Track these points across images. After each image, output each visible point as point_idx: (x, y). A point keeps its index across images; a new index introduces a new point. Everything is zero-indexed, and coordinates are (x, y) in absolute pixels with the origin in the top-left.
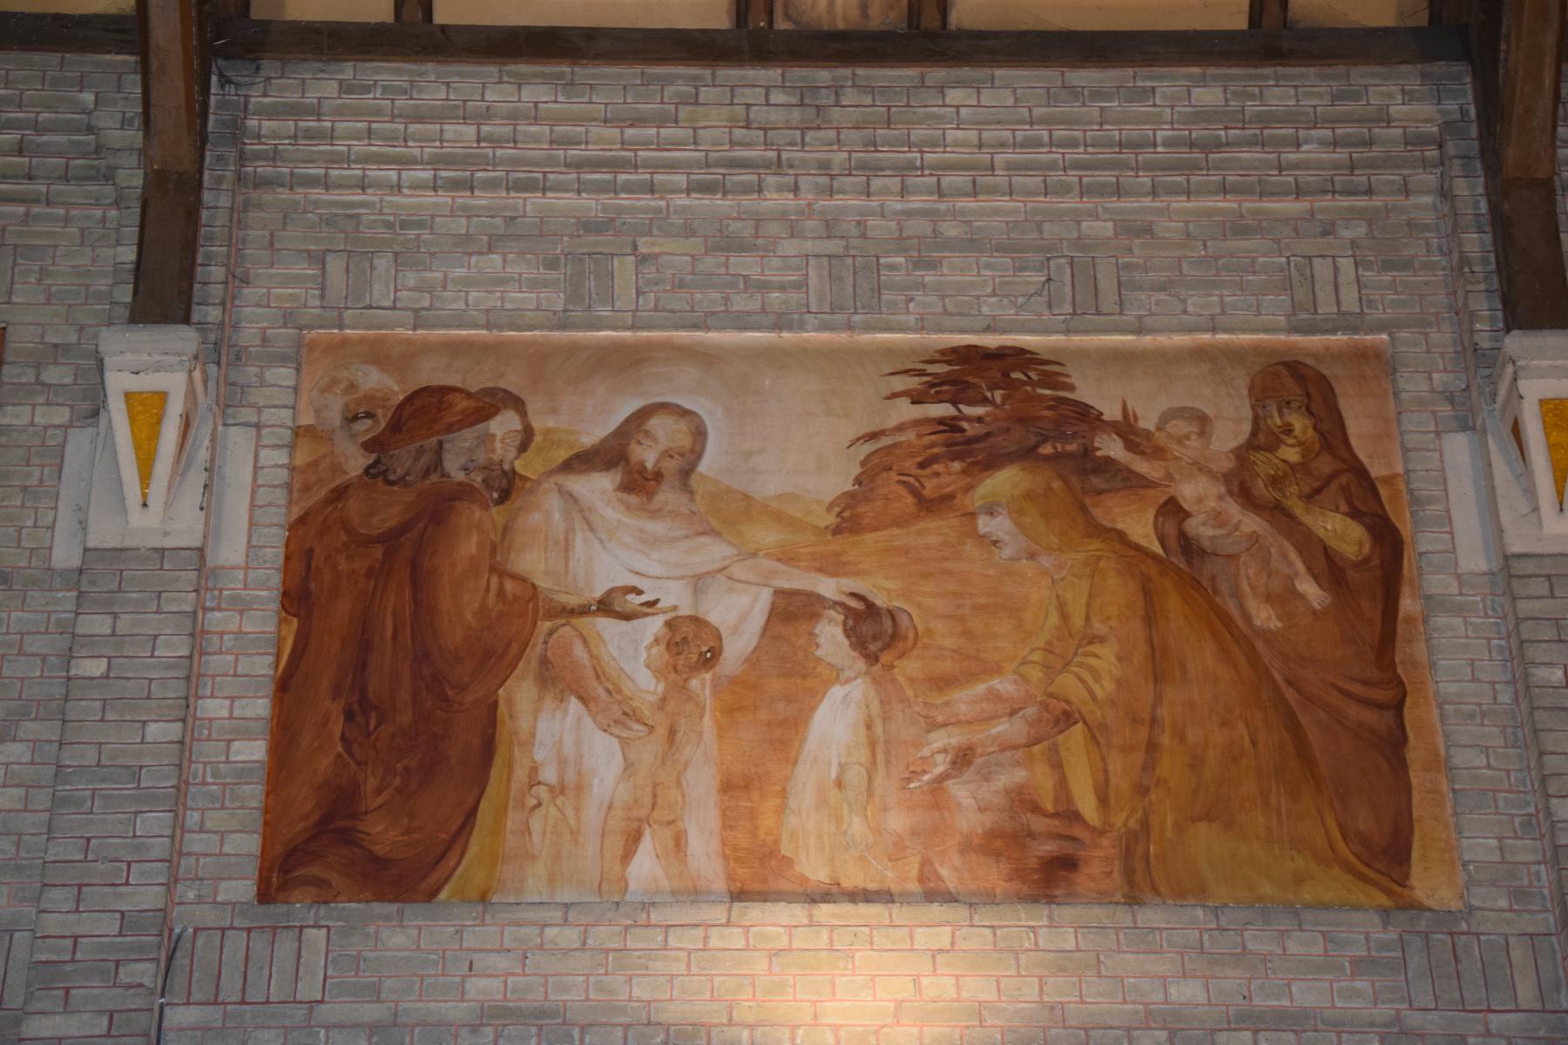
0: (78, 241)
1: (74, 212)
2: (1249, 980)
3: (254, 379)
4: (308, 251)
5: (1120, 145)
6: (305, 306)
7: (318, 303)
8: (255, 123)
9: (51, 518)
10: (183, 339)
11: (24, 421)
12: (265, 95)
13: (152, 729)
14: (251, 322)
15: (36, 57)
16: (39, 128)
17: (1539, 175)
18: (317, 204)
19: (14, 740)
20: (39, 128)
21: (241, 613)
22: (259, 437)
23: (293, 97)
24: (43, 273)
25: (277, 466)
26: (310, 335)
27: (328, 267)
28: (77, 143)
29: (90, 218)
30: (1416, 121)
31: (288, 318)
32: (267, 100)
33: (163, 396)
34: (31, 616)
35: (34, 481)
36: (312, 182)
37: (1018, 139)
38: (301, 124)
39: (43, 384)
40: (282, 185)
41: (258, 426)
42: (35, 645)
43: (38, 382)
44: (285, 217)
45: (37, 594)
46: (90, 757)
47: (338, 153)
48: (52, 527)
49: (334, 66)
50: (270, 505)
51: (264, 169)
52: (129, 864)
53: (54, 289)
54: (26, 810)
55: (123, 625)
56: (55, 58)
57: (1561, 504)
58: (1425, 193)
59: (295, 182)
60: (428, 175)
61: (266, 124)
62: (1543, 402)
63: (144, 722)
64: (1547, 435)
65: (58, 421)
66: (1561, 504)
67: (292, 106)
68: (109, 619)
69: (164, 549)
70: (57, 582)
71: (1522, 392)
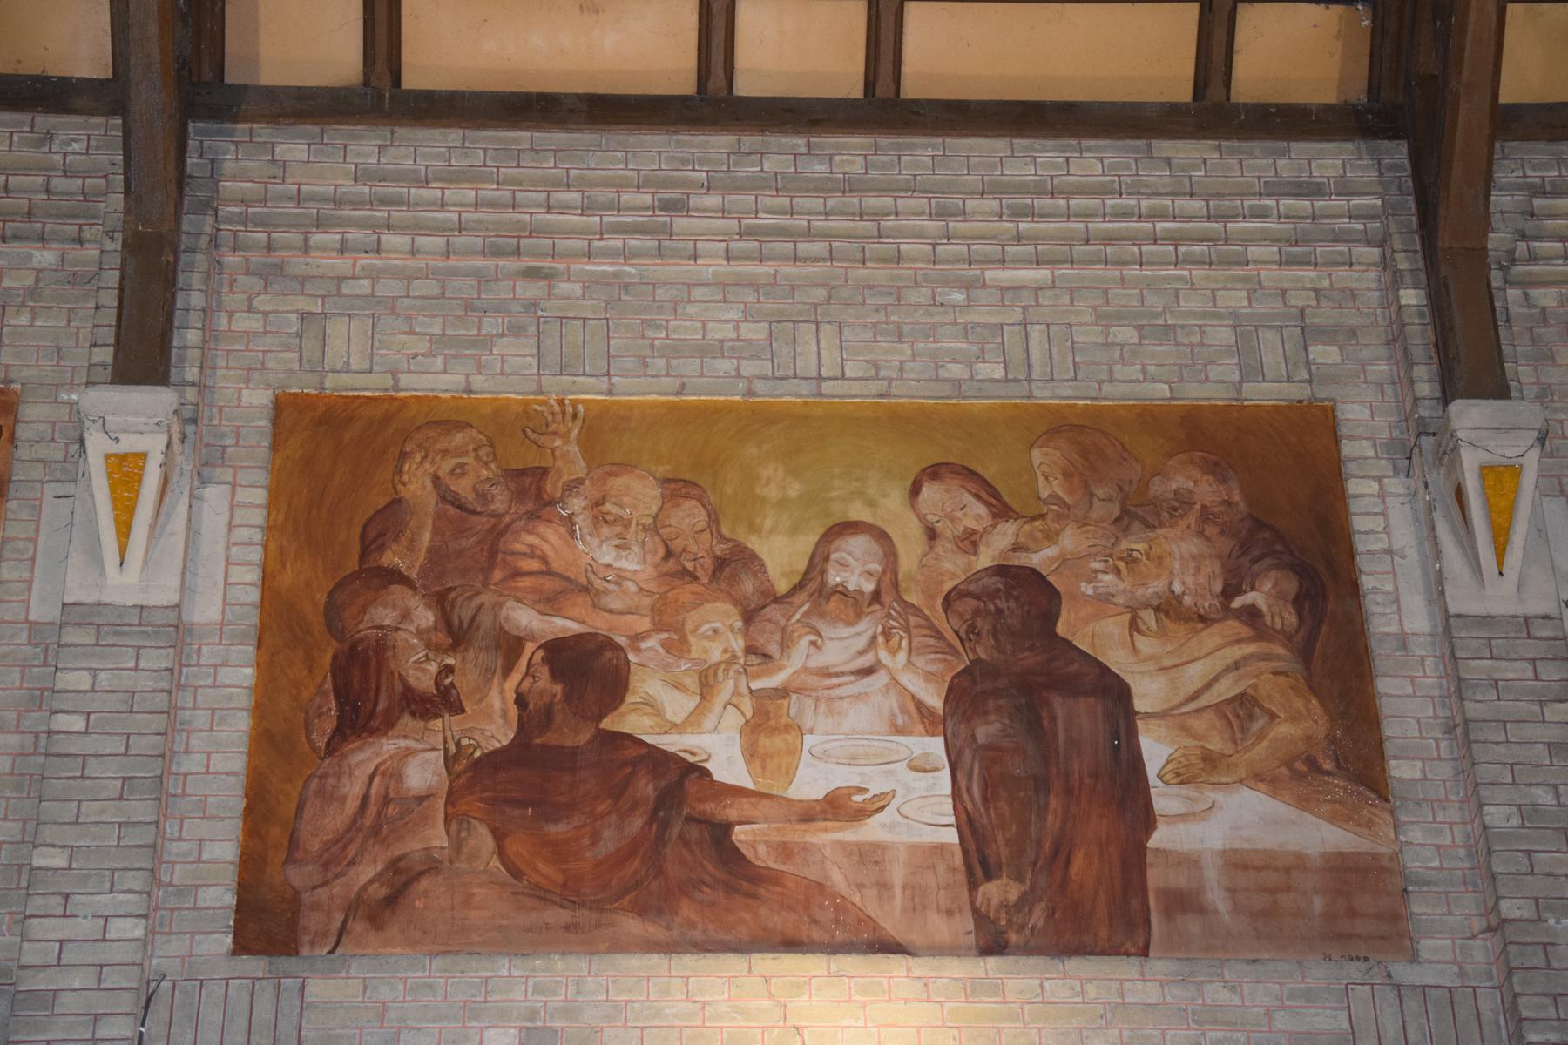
22: (233, 494)
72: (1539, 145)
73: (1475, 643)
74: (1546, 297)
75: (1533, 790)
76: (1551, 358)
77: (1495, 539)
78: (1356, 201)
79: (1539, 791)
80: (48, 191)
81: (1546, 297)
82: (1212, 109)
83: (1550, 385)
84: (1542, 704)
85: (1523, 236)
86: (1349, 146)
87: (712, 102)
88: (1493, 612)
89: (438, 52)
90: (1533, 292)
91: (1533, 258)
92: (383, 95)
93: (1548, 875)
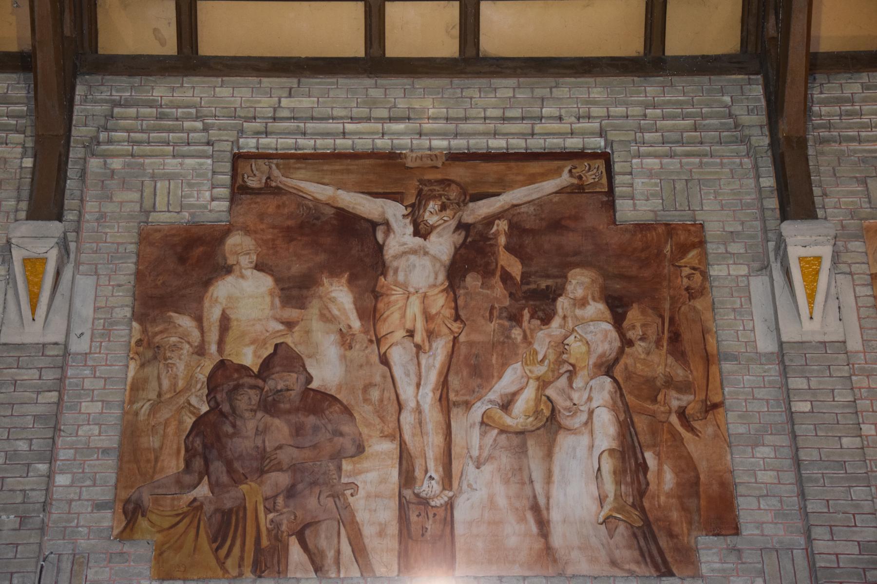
0: (730, 176)
1: (725, 161)
2: (77, 527)
3: (842, 248)
4: (856, 177)
5: (485, 118)
6: (861, 208)
7: (868, 206)
8: (817, 108)
9: (751, 325)
10: (55, 228)
11: (725, 273)
12: (821, 93)
13: (845, 441)
14: (834, 217)
15: (696, 79)
16: (703, 117)
18: (855, 151)
19: (763, 445)
20: (703, 117)
21: (868, 377)
22: (853, 280)
23: (837, 93)
24: (716, 194)
25: (867, 296)
26: (866, 223)
27: (869, 185)
28: (724, 124)
29: (734, 163)
31: (853, 214)
32: (823, 96)
34: (754, 378)
35: (738, 305)
36: (851, 139)
37: (144, 127)
38: (843, 108)
39: (730, 253)
40: (835, 142)
41: (851, 274)
42: (760, 393)
43: (727, 252)
44: (839, 159)
45: (754, 366)
46: (815, 455)
47: (864, 123)
48: (753, 330)
49: (856, 75)
50: (868, 317)
51: (824, 133)
52: (854, 515)
53: (724, 202)
54: (779, 483)
55: (814, 383)
56: (705, 79)
59: (841, 140)
61: (823, 109)
63: (840, 437)
65: (743, 273)
67: (837, 98)
68: (805, 381)
69: (825, 342)
70: (763, 360)
72: (124, 78)
73: (10, 360)
74: (116, 164)
75: (18, 442)
76: (110, 198)
77: (31, 300)
78: (12, 108)
79: (20, 443)
81: (116, 164)
83: (105, 213)
84: (38, 393)
85: (106, 129)
86: (14, 76)
88: (25, 341)
89: (224, 30)
90: (109, 161)
91: (110, 142)
93: (10, 491)
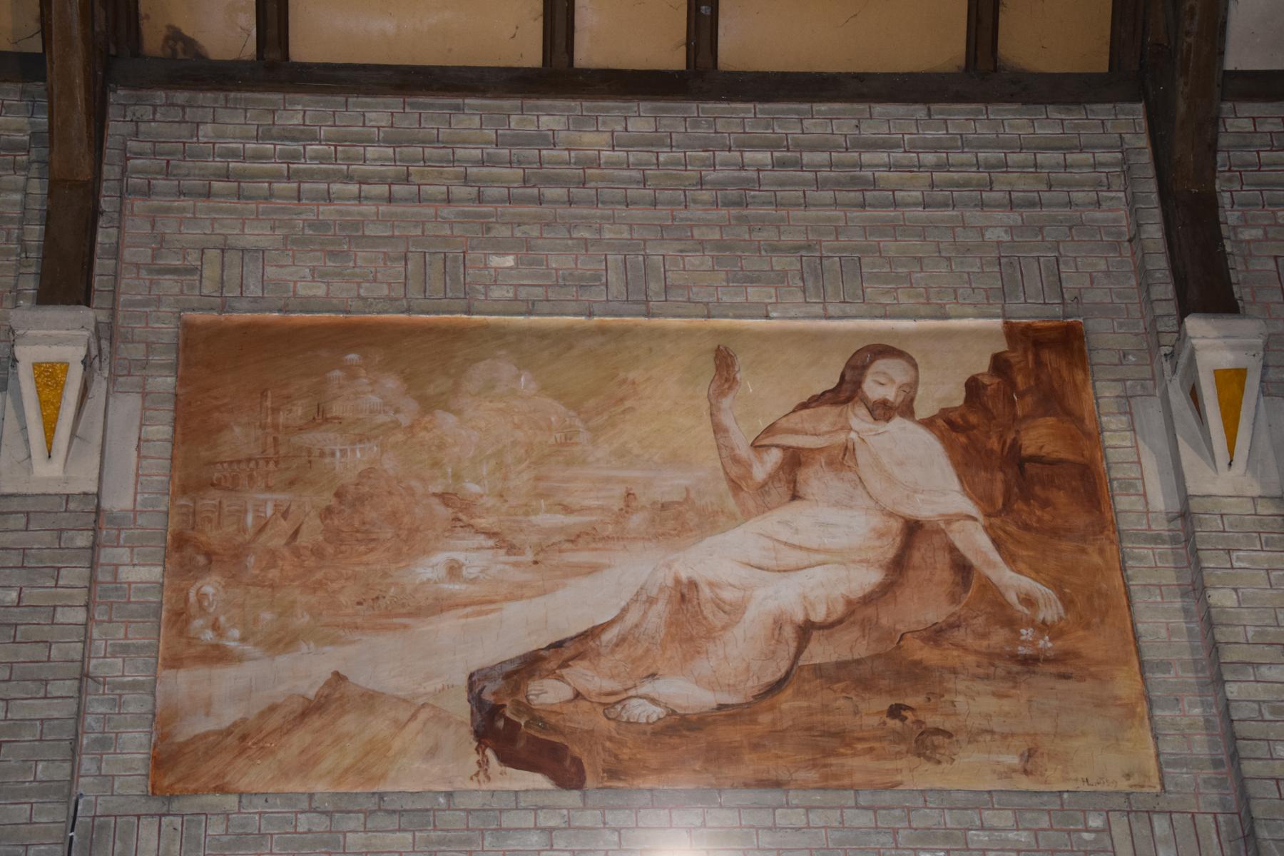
17: (80, 178)
30: (8, 130)
33: (65, 366)
57: (49, 452)
58: (15, 191)
60: (620, 193)
62: (36, 366)
64: (38, 393)
66: (49, 452)
71: (18, 355)
80: (1036, 166)
82: (983, 75)
87: (556, 75)
89: (318, 33)
92: (274, 66)
